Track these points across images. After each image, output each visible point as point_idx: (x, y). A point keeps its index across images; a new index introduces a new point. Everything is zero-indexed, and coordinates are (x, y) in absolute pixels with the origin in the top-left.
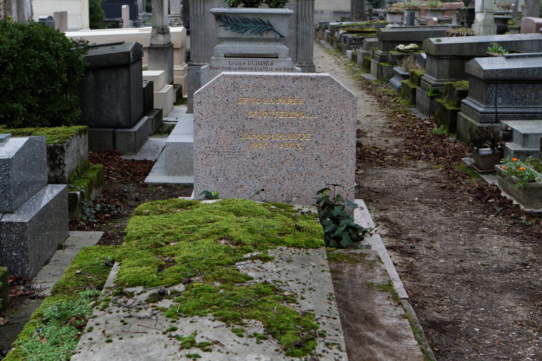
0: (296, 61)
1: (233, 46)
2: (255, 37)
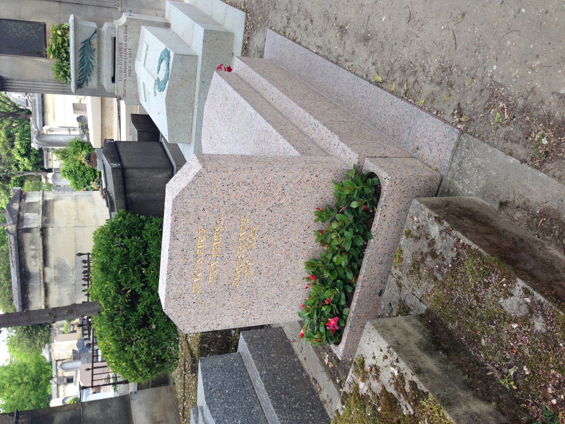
0: (116, 8)
1: (105, 75)
2: (96, 56)
